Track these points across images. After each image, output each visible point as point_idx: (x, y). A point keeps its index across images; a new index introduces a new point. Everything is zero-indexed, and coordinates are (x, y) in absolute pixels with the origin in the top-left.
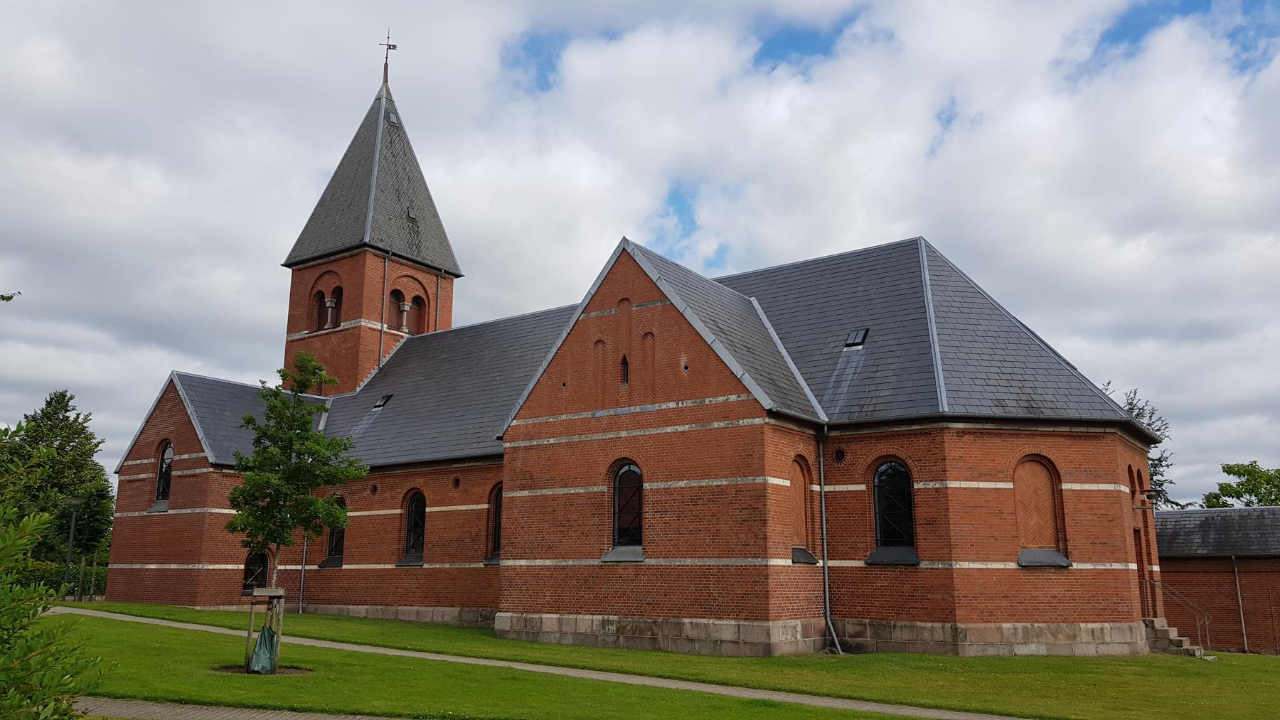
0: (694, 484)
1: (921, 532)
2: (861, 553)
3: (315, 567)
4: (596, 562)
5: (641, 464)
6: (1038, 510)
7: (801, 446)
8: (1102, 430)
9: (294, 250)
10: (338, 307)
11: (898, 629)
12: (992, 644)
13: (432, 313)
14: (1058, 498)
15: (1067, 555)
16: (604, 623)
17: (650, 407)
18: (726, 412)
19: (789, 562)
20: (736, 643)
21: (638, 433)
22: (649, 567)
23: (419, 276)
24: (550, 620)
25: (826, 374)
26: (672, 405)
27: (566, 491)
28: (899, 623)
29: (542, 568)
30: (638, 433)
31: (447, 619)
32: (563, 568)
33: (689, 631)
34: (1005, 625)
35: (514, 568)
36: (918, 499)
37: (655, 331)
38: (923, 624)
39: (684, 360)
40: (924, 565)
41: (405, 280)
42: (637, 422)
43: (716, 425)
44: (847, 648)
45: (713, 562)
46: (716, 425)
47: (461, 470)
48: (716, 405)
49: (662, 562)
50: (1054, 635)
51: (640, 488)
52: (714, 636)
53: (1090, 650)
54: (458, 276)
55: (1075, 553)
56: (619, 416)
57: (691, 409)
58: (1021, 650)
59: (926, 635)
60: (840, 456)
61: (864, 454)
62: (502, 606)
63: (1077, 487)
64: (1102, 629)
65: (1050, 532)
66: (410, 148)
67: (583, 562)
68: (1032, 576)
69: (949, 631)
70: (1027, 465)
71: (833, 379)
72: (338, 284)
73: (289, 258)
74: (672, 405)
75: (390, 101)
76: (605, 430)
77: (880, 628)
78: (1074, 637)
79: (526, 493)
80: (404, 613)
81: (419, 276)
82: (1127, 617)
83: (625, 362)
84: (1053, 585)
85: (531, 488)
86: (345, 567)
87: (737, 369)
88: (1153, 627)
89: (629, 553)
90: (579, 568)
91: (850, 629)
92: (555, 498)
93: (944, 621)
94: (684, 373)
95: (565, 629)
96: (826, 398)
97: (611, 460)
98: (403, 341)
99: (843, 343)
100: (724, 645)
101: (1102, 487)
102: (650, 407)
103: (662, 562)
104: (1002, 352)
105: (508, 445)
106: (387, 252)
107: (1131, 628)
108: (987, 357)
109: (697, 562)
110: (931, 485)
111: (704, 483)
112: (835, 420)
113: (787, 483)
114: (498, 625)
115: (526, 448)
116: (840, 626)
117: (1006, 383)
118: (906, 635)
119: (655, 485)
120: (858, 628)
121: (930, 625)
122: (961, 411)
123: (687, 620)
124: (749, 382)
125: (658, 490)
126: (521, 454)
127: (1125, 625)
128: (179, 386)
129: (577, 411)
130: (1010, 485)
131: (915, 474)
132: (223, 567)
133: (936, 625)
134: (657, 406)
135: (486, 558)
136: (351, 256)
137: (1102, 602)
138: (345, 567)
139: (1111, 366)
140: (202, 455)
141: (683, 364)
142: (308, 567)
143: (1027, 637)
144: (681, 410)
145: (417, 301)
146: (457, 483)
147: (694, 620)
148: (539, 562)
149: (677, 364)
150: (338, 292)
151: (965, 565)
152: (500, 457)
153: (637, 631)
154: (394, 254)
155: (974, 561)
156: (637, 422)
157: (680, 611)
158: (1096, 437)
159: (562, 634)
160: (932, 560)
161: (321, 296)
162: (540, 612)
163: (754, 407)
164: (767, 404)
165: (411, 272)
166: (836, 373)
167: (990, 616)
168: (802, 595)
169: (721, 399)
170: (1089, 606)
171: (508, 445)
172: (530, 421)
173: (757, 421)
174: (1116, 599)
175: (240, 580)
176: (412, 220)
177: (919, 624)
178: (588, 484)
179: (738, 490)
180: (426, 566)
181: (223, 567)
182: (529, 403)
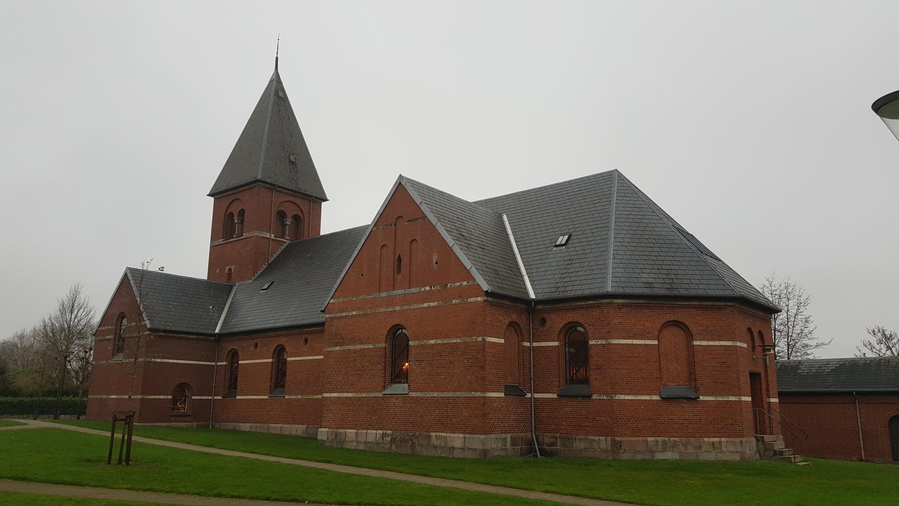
3: (220, 398)
4: (380, 395)
7: (515, 316)
8: (724, 304)
10: (242, 222)
12: (640, 452)
13: (306, 225)
15: (696, 390)
16: (384, 435)
19: (502, 395)
22: (412, 398)
23: (297, 201)
27: (362, 347)
28: (578, 437)
29: (347, 398)
32: (360, 398)
33: (434, 441)
34: (649, 439)
35: (330, 398)
37: (418, 238)
38: (593, 438)
40: (595, 397)
41: (287, 204)
42: (405, 299)
44: (543, 453)
45: (450, 394)
47: (307, 333)
52: (450, 444)
53: (711, 456)
58: (660, 456)
60: (543, 322)
61: (558, 321)
63: (705, 343)
64: (720, 442)
69: (609, 442)
78: (700, 447)
79: (338, 348)
81: (297, 201)
82: (740, 434)
85: (341, 344)
86: (238, 397)
87: (468, 264)
88: (763, 441)
89: (400, 388)
91: (547, 440)
92: (355, 351)
93: (607, 435)
94: (435, 266)
95: (360, 439)
98: (285, 245)
101: (723, 343)
104: (658, 250)
105: (328, 316)
107: (741, 442)
108: (646, 253)
109: (441, 394)
110: (600, 342)
112: (541, 297)
113: (502, 341)
116: (541, 440)
117: (657, 271)
119: (416, 343)
123: (433, 434)
124: (475, 273)
127: (738, 440)
128: (130, 277)
130: (656, 342)
131: (590, 335)
132: (157, 397)
133: (601, 438)
137: (723, 422)
138: (238, 397)
139: (753, 264)
141: (435, 261)
143: (665, 447)
145: (296, 218)
146: (306, 341)
147: (438, 434)
148: (345, 395)
149: (432, 261)
150: (242, 213)
151: (622, 397)
152: (322, 324)
155: (629, 394)
158: (720, 308)
159: (358, 443)
160: (600, 394)
161: (232, 214)
163: (476, 289)
164: (485, 287)
165: (292, 199)
168: (512, 417)
169: (457, 284)
171: (328, 316)
173: (479, 299)
176: (292, 163)
180: (287, 397)
181: (157, 397)
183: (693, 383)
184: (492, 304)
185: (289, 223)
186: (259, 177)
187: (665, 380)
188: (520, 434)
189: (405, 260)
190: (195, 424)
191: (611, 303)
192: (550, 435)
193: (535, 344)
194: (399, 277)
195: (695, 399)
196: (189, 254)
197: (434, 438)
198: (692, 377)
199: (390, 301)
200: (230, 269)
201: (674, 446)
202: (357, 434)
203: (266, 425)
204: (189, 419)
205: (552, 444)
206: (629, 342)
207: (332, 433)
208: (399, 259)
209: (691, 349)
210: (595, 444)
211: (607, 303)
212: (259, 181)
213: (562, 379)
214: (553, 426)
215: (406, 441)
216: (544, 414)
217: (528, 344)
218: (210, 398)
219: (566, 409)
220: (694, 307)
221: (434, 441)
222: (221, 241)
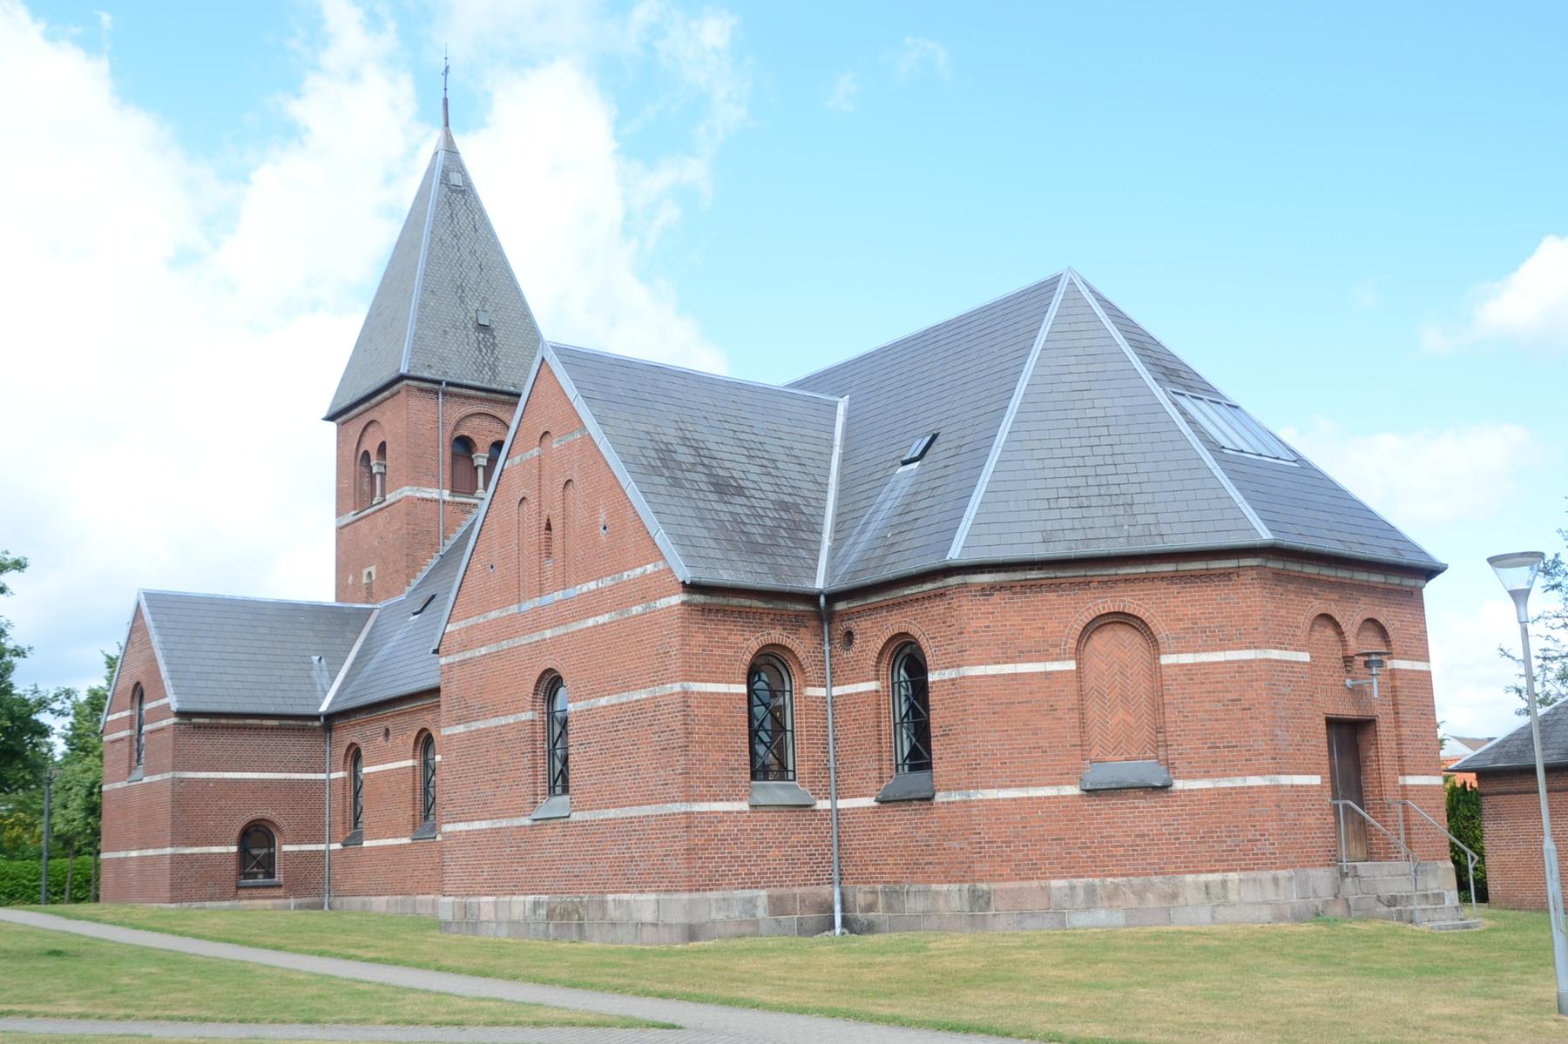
2: (873, 785)
4: (526, 821)
9: (336, 396)
11: (911, 896)
12: (1033, 915)
15: (1170, 766)
16: (537, 905)
20: (655, 925)
22: (576, 824)
26: (592, 585)
28: (914, 888)
33: (614, 913)
34: (1055, 883)
40: (940, 797)
41: (476, 421)
42: (562, 614)
50: (1140, 894)
56: (543, 608)
60: (849, 636)
61: (874, 633)
63: (1187, 658)
64: (1224, 883)
69: (966, 894)
77: (894, 895)
78: (1175, 896)
79: (460, 729)
84: (1142, 814)
89: (558, 805)
100: (645, 929)
106: (439, 383)
107: (1276, 880)
113: (1305, 657)
115: (463, 663)
116: (850, 898)
120: (870, 898)
123: (610, 897)
126: (456, 672)
127: (1266, 875)
131: (930, 661)
132: (205, 850)
137: (1231, 839)
148: (477, 825)
150: (382, 448)
154: (449, 384)
156: (562, 614)
158: (1225, 575)
161: (366, 453)
167: (1029, 870)
170: (1203, 847)
175: (232, 866)
176: (484, 328)
177: (934, 887)
181: (205, 850)
183: (1161, 752)
184: (705, 610)
186: (404, 370)
187: (1097, 749)
188: (797, 890)
189: (556, 525)
190: (292, 901)
191: (965, 585)
192: (867, 888)
193: (837, 691)
194: (549, 564)
195: (1165, 788)
196: (289, 549)
197: (611, 905)
198: (1160, 739)
201: (1113, 895)
203: (410, 899)
204: (281, 892)
208: (549, 527)
209: (1156, 670)
210: (941, 902)
211: (960, 586)
212: (402, 378)
213: (886, 764)
214: (871, 869)
217: (821, 692)
218: (322, 847)
220: (1163, 577)
221: (614, 913)
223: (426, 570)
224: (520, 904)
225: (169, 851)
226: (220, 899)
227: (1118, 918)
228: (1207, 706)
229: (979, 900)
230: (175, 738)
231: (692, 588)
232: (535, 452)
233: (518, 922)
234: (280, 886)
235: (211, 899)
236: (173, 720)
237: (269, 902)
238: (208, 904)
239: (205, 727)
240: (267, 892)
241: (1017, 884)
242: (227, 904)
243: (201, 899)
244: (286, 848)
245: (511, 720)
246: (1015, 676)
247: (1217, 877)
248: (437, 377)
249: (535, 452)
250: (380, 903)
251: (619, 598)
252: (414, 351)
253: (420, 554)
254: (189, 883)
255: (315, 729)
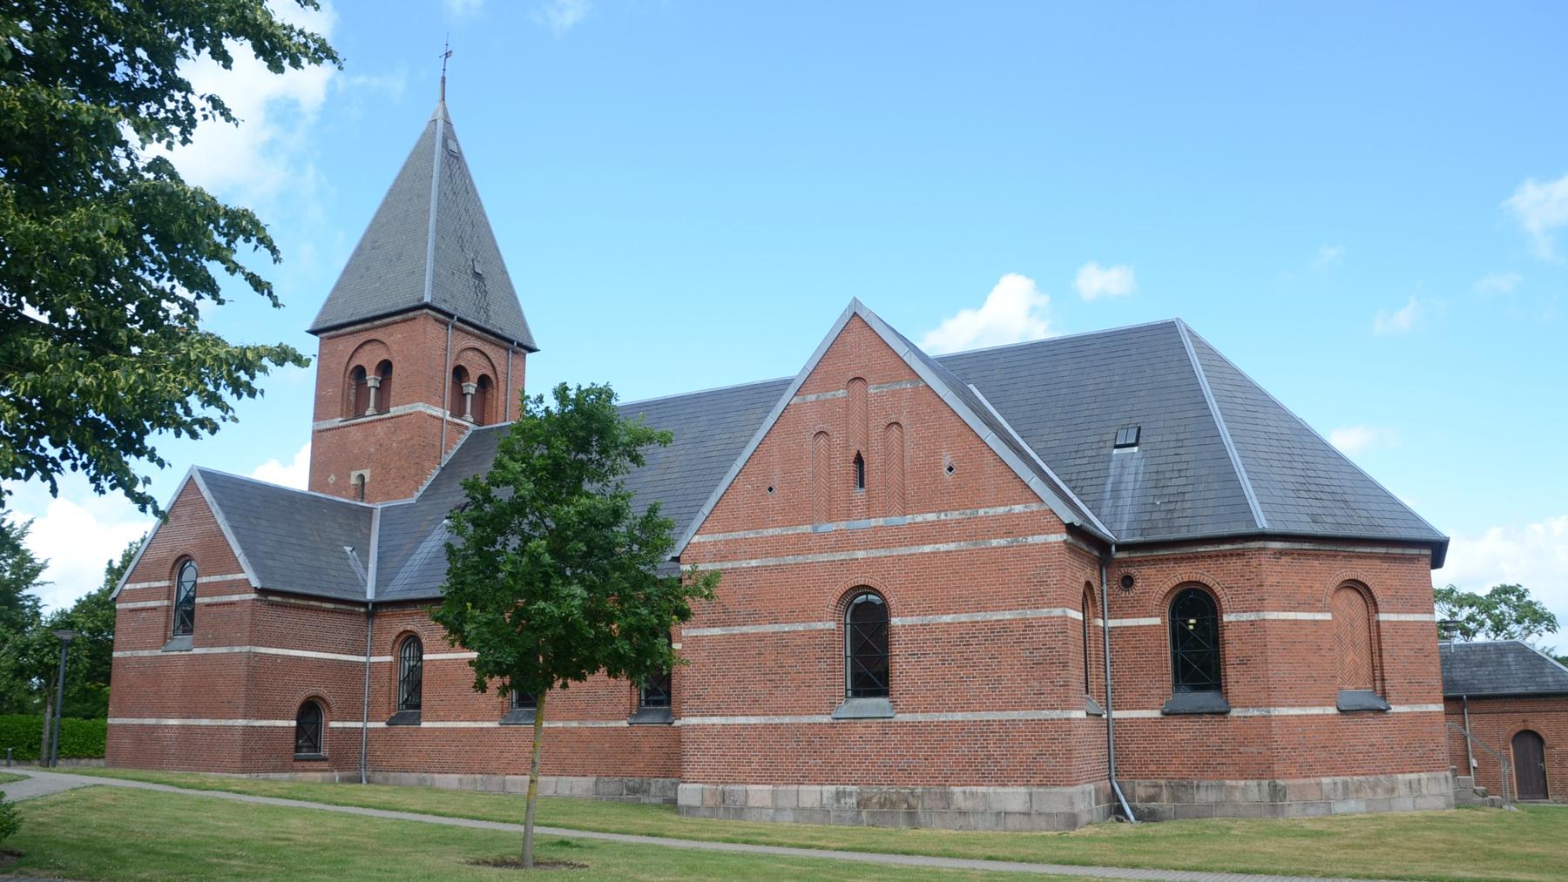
0: (963, 618)
1: (1231, 674)
2: (1156, 701)
3: (382, 725)
4: (826, 719)
5: (882, 589)
6: (1354, 645)
11: (1202, 790)
14: (1375, 630)
15: (1384, 695)
16: (839, 796)
17: (897, 520)
18: (1009, 527)
21: (882, 553)
22: (902, 725)
24: (759, 794)
25: (1099, 481)
26: (931, 517)
28: (1204, 783)
29: (745, 727)
30: (882, 553)
31: (577, 791)
32: (776, 727)
34: (1325, 780)
36: (1228, 635)
37: (903, 422)
38: (1234, 783)
39: (947, 460)
40: (1235, 712)
41: (470, 353)
42: (876, 538)
43: (994, 543)
46: (994, 543)
48: (995, 518)
49: (920, 717)
50: (1373, 789)
51: (887, 622)
52: (996, 807)
54: (532, 350)
55: (1393, 695)
56: (853, 532)
57: (958, 522)
59: (1237, 796)
60: (1128, 582)
61: (1159, 581)
62: (687, 775)
65: (1365, 671)
66: (472, 184)
67: (805, 719)
68: (1352, 723)
70: (1343, 593)
71: (1108, 487)
72: (385, 357)
73: (317, 322)
74: (931, 517)
75: (448, 123)
76: (832, 549)
77: (1180, 788)
78: (1392, 790)
79: (717, 631)
80: (514, 784)
81: (487, 348)
83: (859, 460)
85: (724, 624)
90: (798, 727)
91: (1141, 792)
92: (761, 637)
94: (947, 475)
95: (781, 803)
96: (1105, 511)
97: (842, 587)
98: (468, 433)
99: (1110, 444)
100: (1010, 819)
102: (897, 520)
103: (920, 717)
106: (451, 316)
109: (970, 716)
111: (979, 617)
112: (1124, 539)
114: (682, 801)
116: (1129, 791)
118: (1212, 797)
119: (909, 621)
120: (1152, 791)
121: (1242, 783)
122: (1280, 528)
125: (912, 627)
129: (790, 524)
131: (1224, 604)
133: (1249, 782)
134: (908, 519)
135: (631, 715)
136: (404, 321)
140: (240, 576)
142: (371, 725)
144: (945, 524)
145: (484, 381)
147: (968, 789)
150: (385, 368)
153: (887, 803)
154: (460, 320)
157: (946, 778)
161: (360, 372)
162: (744, 782)
166: (1110, 480)
167: (1308, 770)
169: (1001, 510)
172: (721, 537)
174: (1432, 746)
176: (477, 275)
177: (1228, 782)
178: (810, 619)
179: (1028, 625)
182: (718, 513)
185: (472, 391)
186: (427, 299)
190: (337, 775)
191: (1264, 549)
192: (1147, 782)
198: (1378, 674)
199: (844, 541)
200: (362, 477)
202: (774, 794)
203: (498, 778)
204: (324, 765)
205: (1152, 798)
206: (1291, 616)
207: (713, 793)
211: (1259, 549)
212: (427, 306)
215: (893, 804)
216: (1133, 747)
218: (360, 725)
219: (1178, 737)
222: (336, 422)
223: (431, 479)
224: (812, 794)
225: (241, 722)
226: (282, 770)
227: (1362, 806)
228: (1406, 652)
229: (1276, 792)
230: (253, 613)
231: (1070, 528)
232: (841, 393)
233: (812, 809)
234: (325, 759)
235: (274, 770)
236: (254, 596)
237: (319, 775)
238: (272, 775)
239: (277, 605)
240: (316, 765)
241: (1301, 781)
242: (286, 775)
243: (266, 771)
244: (333, 724)
245: (800, 627)
246: (1296, 622)
247: (1413, 776)
248: (451, 311)
249: (841, 393)
250: (451, 780)
251: (967, 530)
252: (434, 286)
253: (427, 464)
254: (257, 755)
255: (359, 614)
